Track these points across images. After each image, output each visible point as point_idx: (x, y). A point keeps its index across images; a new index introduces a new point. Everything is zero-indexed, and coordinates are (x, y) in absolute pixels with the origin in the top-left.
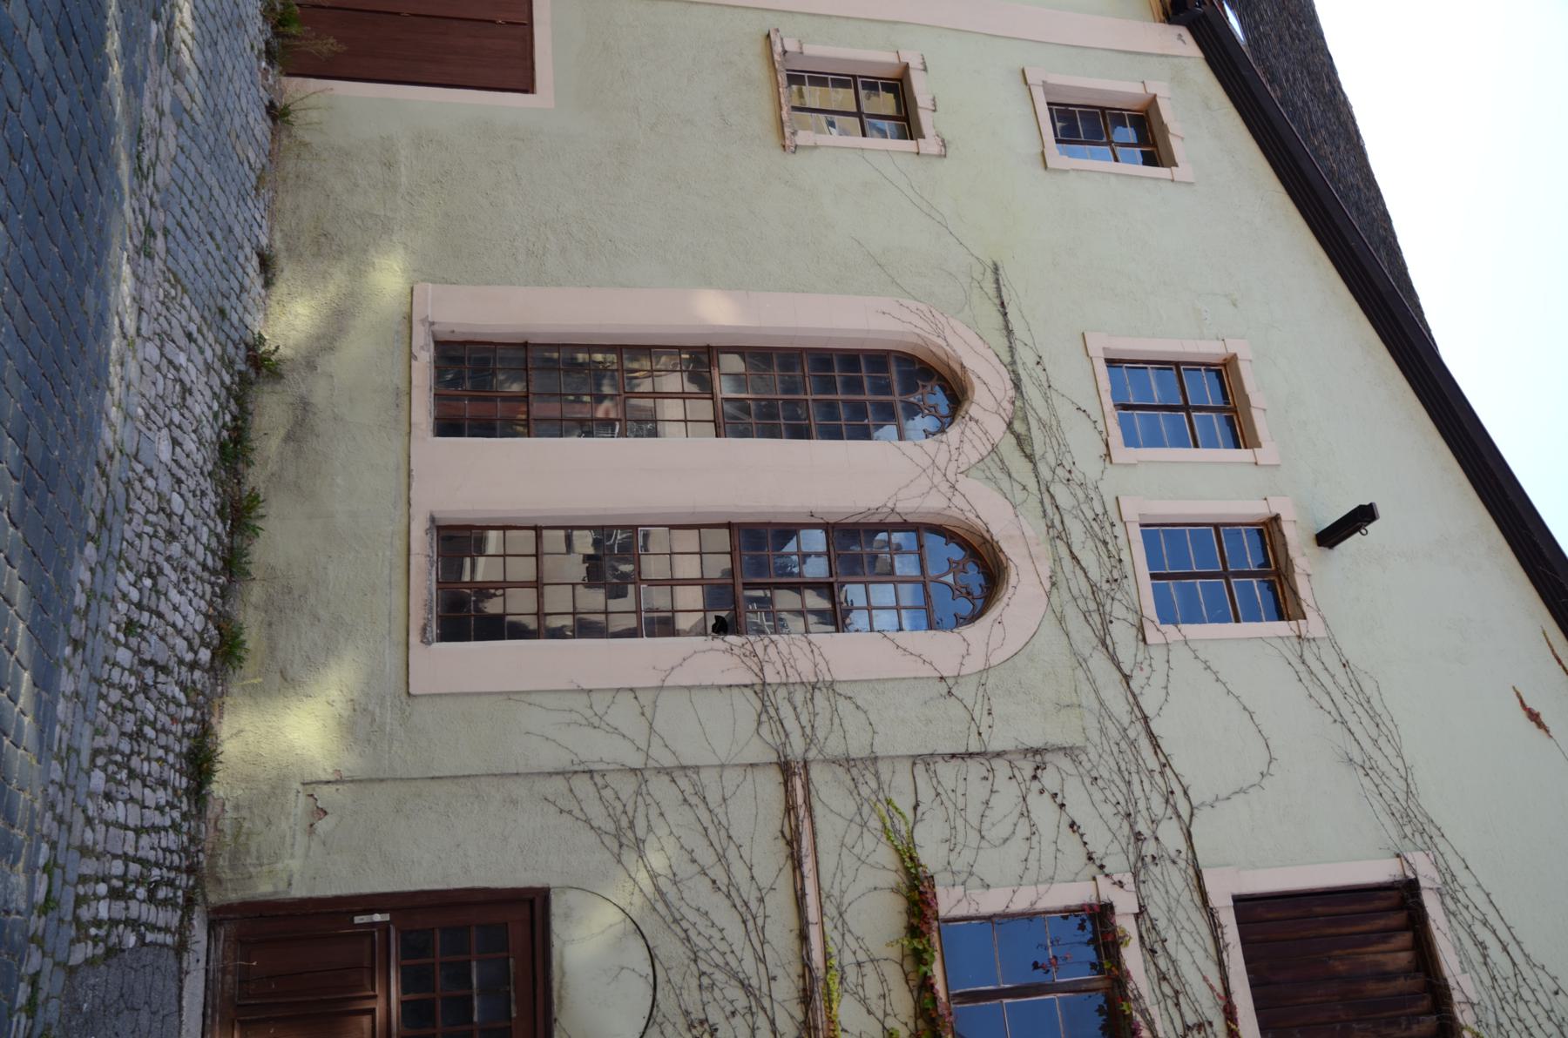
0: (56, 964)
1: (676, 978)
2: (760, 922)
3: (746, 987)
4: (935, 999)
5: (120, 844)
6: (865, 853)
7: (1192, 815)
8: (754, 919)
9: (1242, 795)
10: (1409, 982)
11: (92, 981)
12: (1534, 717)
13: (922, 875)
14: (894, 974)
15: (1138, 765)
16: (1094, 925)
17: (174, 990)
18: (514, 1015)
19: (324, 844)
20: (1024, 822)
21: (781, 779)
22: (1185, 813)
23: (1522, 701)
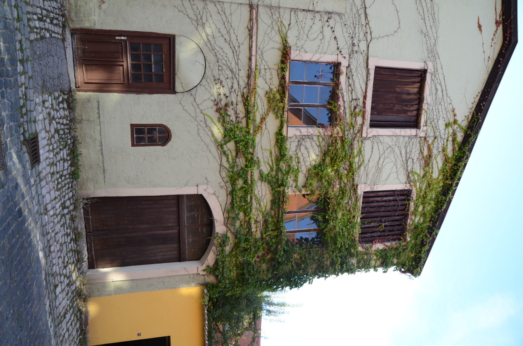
0: (26, 38)
1: (212, 66)
2: (238, 53)
3: (232, 71)
4: (285, 82)
5: (38, 3)
6: (272, 37)
7: (371, 41)
8: (236, 52)
9: (387, 37)
10: (415, 96)
11: (38, 46)
12: (480, 27)
13: (288, 46)
14: (275, 73)
15: (359, 22)
16: (334, 68)
17: (64, 52)
18: (164, 71)
19: (105, 12)
20: (321, 34)
21: (249, 10)
22: (369, 40)
23: (478, 21)
